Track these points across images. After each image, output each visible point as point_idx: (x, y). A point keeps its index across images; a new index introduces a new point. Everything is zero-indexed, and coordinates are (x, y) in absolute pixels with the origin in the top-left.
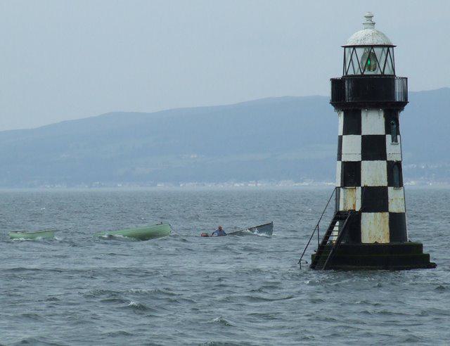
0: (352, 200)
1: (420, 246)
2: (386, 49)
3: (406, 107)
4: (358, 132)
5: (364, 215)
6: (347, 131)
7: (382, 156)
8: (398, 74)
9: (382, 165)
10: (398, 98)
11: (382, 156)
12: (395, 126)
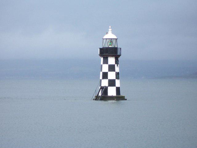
0: (105, 83)
7: (114, 70)
10: (118, 54)
11: (114, 70)
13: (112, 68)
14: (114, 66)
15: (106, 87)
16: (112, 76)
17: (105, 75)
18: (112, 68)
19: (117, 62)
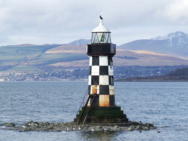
0: (96, 89)
1: (119, 108)
6: (94, 64)
12: (111, 62)
14: (107, 67)
16: (104, 80)
17: (95, 80)
18: (104, 70)
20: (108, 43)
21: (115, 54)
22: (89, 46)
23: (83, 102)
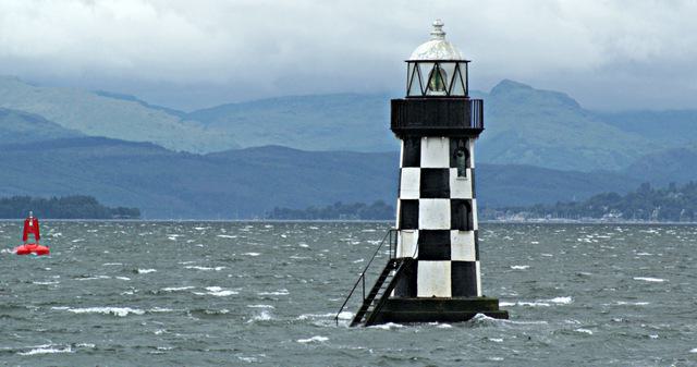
2: (412, 65)
3: (481, 135)
4: (455, 265)
5: (420, 263)
8: (472, 96)
9: (444, 267)
12: (463, 158)
13: (434, 184)
15: (448, 191)
16: (435, 214)
17: (410, 211)
18: (434, 184)
19: (459, 156)
20: (451, 94)
21: (481, 130)
22: (396, 104)
23: (361, 283)
